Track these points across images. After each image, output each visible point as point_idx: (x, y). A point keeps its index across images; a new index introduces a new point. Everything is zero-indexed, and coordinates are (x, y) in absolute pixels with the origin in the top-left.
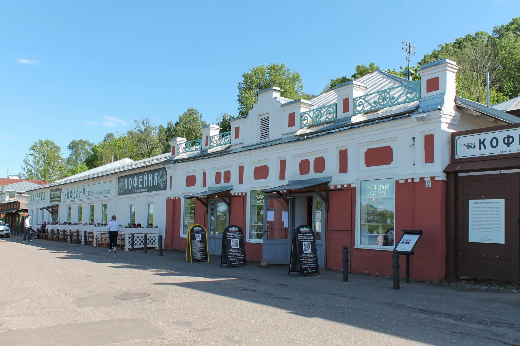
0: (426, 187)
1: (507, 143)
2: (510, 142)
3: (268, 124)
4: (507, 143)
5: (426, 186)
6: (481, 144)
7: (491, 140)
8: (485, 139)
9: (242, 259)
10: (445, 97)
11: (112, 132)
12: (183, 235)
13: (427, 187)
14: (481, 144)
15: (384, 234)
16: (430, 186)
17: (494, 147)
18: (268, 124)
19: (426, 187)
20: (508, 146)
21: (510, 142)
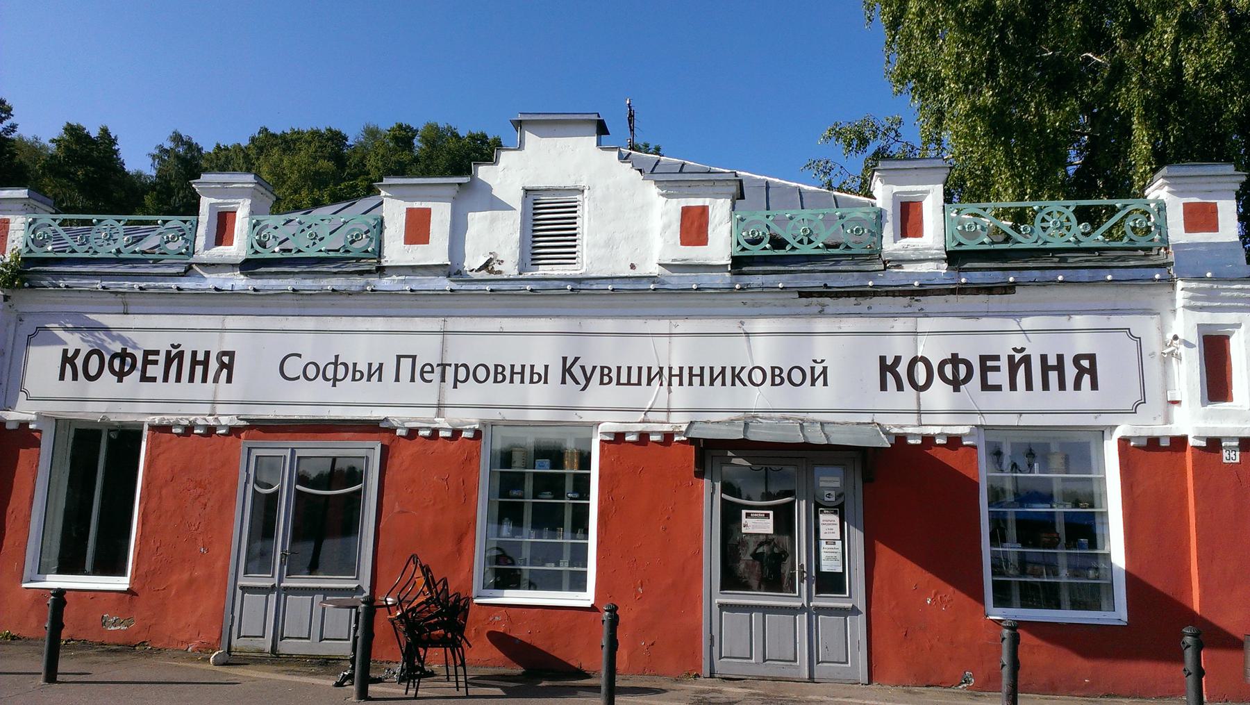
0: (1225, 461)
1: (117, 370)
2: (127, 368)
3: (574, 221)
4: (117, 370)
5: (1224, 458)
6: (67, 364)
7: (279, 364)
8: (80, 350)
9: (825, 479)
10: (1076, 222)
11: (399, 122)
12: (370, 453)
13: (1227, 461)
14: (67, 364)
15: (1095, 478)
16: (1238, 460)
17: (90, 378)
18: (574, 221)
19: (1225, 461)
20: (120, 380)
21: (339, 377)
